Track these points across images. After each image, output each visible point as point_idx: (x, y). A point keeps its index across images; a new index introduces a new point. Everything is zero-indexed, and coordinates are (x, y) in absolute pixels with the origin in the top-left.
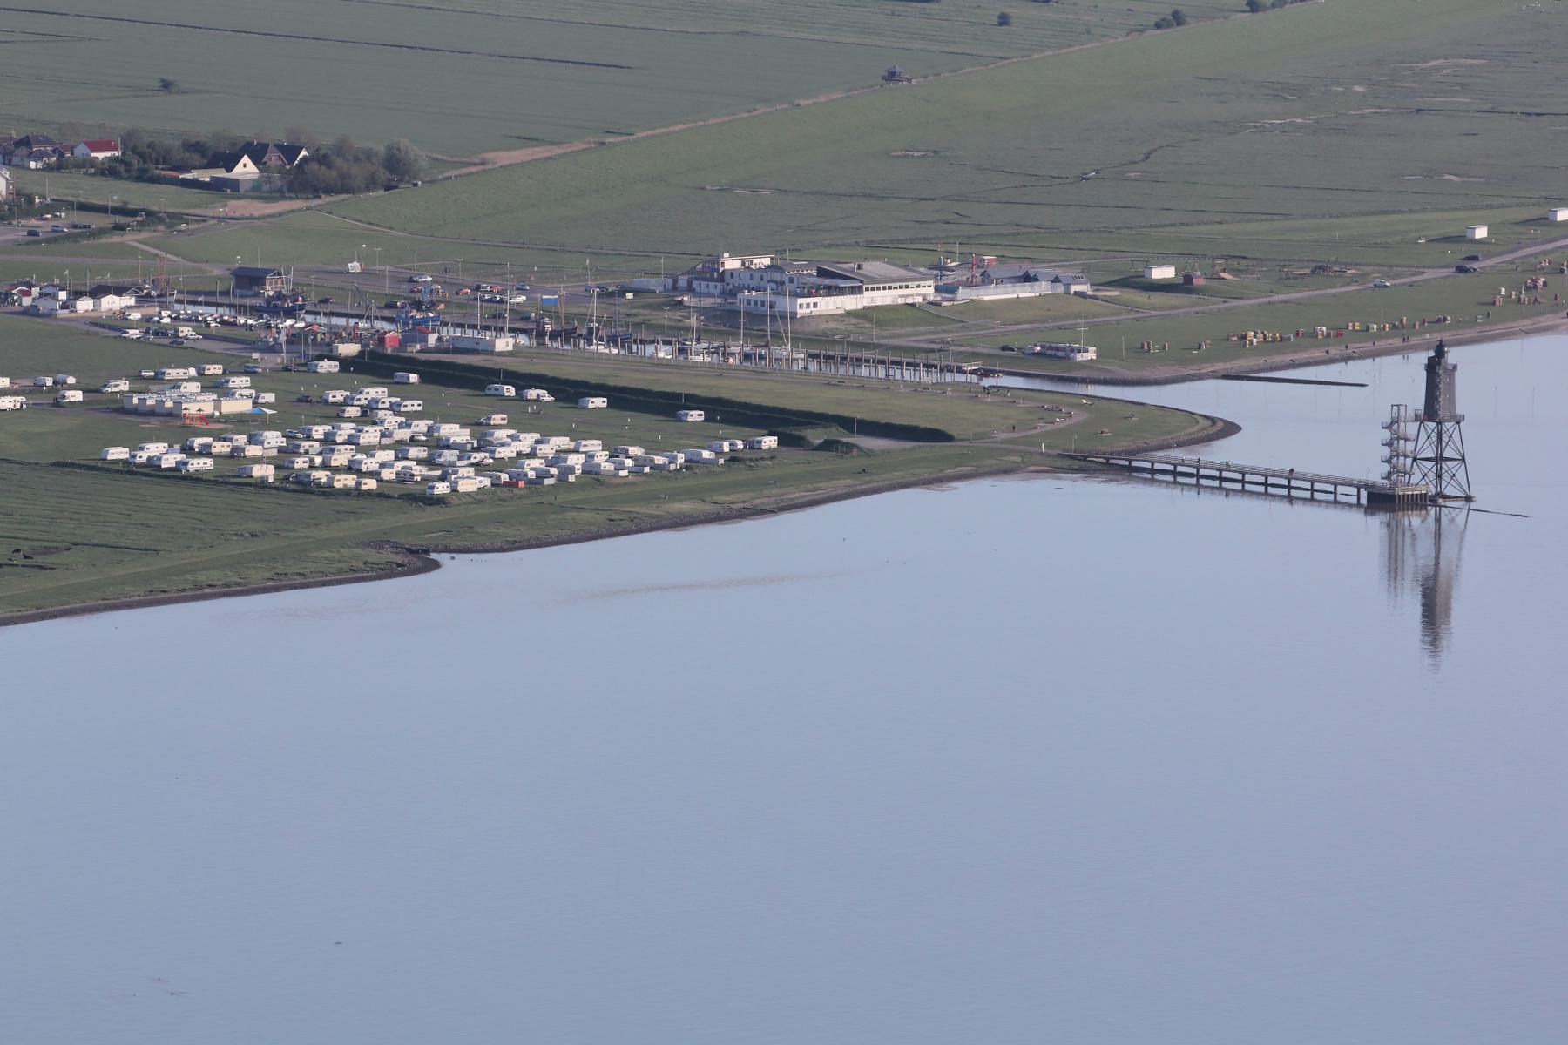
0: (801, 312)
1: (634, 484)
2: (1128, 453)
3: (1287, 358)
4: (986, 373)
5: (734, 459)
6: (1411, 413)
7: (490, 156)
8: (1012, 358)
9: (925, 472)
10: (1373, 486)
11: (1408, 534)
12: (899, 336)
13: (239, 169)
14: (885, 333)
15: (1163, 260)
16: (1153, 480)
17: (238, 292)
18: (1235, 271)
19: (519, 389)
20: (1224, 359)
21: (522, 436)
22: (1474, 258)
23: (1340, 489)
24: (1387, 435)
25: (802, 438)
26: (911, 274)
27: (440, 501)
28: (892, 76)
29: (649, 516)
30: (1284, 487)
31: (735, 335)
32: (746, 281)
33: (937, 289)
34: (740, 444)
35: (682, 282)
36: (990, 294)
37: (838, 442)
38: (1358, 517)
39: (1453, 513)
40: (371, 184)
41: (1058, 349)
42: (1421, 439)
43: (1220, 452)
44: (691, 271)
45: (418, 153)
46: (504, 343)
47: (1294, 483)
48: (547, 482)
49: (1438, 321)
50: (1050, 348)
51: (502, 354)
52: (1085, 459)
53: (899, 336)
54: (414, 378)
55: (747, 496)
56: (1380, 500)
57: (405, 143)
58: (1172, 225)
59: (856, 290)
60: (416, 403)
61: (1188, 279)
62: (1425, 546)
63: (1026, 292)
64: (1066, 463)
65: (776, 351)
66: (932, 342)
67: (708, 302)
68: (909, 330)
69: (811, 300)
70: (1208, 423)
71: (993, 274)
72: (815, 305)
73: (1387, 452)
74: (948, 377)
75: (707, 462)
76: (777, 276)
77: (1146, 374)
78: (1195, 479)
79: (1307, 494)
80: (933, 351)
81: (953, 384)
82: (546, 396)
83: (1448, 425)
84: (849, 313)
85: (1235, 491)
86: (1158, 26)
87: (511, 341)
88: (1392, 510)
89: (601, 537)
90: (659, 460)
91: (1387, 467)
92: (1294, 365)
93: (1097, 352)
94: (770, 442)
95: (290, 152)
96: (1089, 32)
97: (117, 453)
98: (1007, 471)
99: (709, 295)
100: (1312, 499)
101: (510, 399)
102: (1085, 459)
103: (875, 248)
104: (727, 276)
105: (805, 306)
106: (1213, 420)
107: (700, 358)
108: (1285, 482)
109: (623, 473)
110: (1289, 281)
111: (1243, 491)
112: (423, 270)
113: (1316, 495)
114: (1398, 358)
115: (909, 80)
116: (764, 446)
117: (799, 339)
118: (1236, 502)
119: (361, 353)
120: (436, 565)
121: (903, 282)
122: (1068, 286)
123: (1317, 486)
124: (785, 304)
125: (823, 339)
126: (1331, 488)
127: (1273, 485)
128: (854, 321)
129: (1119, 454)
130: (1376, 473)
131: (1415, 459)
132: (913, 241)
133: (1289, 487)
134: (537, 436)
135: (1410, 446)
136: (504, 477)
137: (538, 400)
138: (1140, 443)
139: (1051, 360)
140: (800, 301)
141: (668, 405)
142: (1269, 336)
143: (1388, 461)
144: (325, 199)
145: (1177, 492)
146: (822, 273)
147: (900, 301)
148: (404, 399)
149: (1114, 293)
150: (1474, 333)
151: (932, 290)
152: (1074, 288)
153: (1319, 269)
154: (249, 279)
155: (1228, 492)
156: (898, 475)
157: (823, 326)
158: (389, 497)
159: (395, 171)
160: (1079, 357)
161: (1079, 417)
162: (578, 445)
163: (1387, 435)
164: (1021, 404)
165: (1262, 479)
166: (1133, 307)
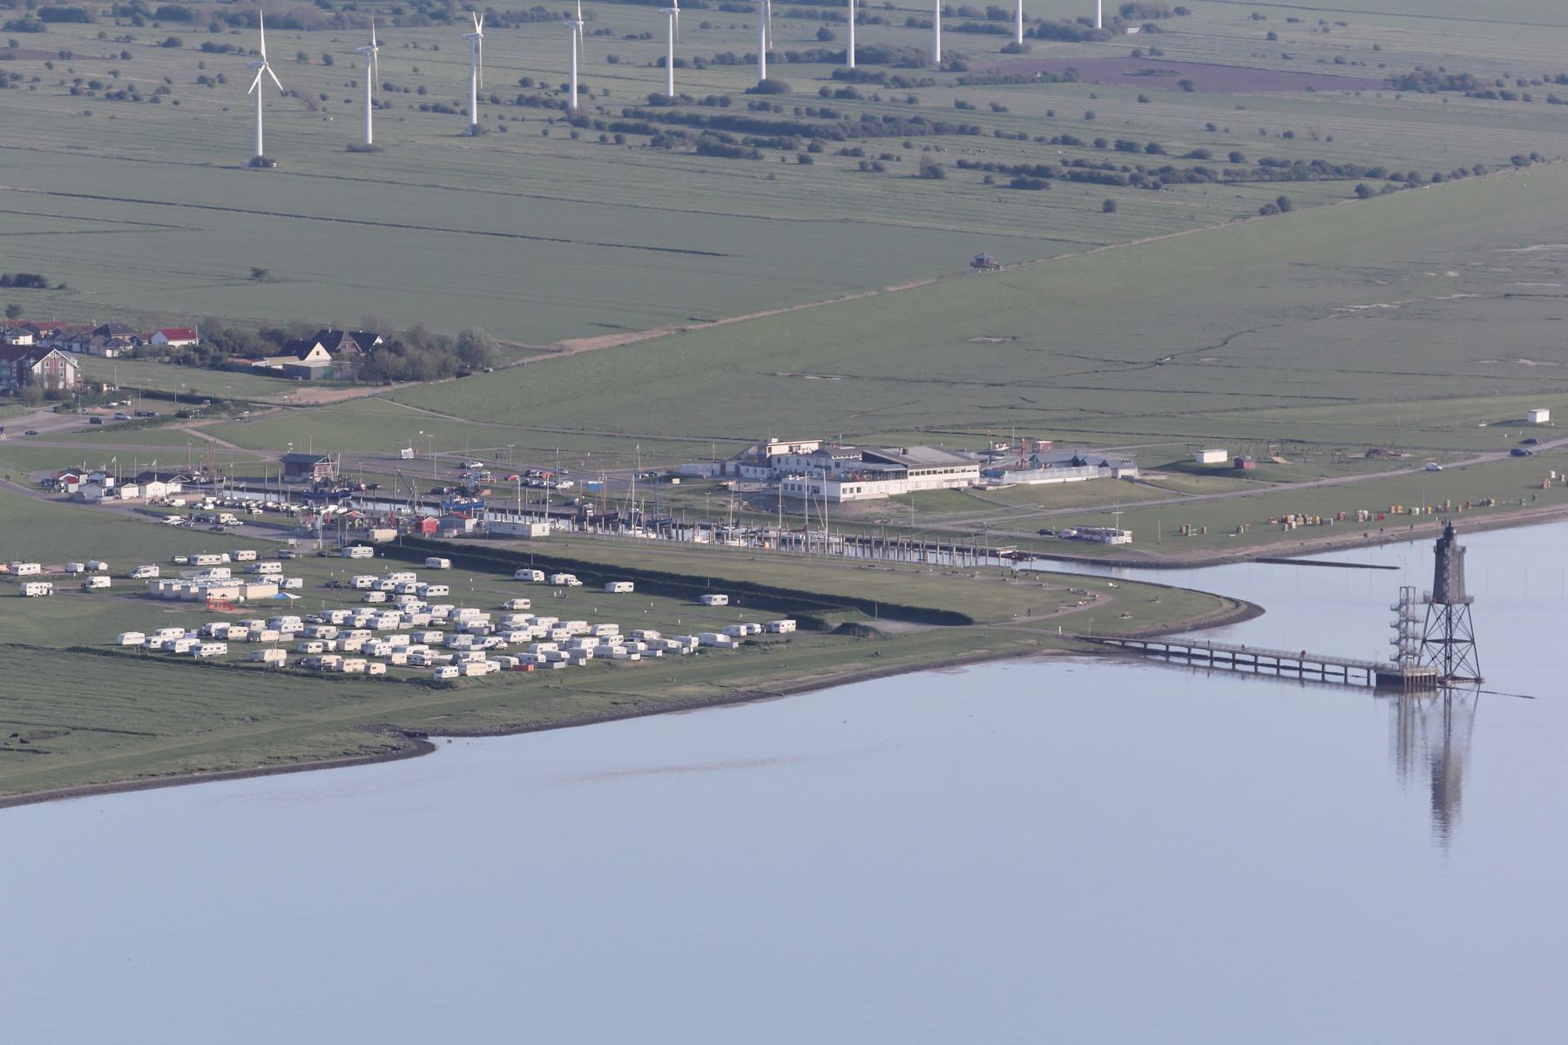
0: (844, 497)
1: (644, 667)
3: (1324, 541)
4: (1020, 557)
5: (748, 643)
6: (1420, 596)
8: (1049, 542)
9: (939, 655)
10: (1383, 668)
11: (1418, 716)
12: (940, 520)
13: (312, 356)
15: (1216, 444)
19: (548, 573)
20: (1260, 543)
21: (540, 620)
22: (1531, 442)
23: (1351, 671)
24: (1395, 617)
26: (957, 459)
27: (448, 685)
28: (980, 263)
29: (655, 700)
30: (1296, 669)
31: (774, 520)
32: (793, 465)
33: (984, 474)
34: (757, 628)
35: (730, 467)
36: (1037, 479)
38: (1368, 698)
39: (1463, 694)
40: (443, 370)
41: (1094, 533)
42: (1430, 621)
43: (1242, 635)
44: (737, 458)
45: (489, 338)
46: (540, 529)
47: (1305, 665)
48: (557, 665)
49: (1482, 504)
50: (1087, 532)
51: (538, 539)
52: (1101, 642)
53: (940, 520)
54: (445, 563)
56: (1389, 682)
58: (1236, 410)
59: (900, 475)
60: (442, 587)
61: (1239, 463)
62: (1435, 728)
63: (1074, 476)
64: (1082, 645)
66: (968, 525)
67: (754, 487)
68: (951, 514)
69: (855, 485)
70: (1232, 605)
72: (859, 490)
73: (1395, 634)
75: (721, 646)
76: (823, 462)
77: (1179, 557)
78: (1209, 661)
80: (969, 535)
82: (573, 581)
84: (893, 498)
86: (1263, 212)
93: (1133, 536)
94: (788, 626)
95: (364, 340)
97: (133, 638)
99: (756, 480)
101: (539, 583)
102: (1101, 642)
103: (932, 433)
104: (774, 462)
105: (848, 491)
106: (1237, 603)
107: (735, 543)
108: (1297, 665)
109: (635, 657)
116: (782, 630)
119: (397, 538)
121: (948, 466)
122: (1115, 470)
124: (826, 489)
125: (865, 523)
126: (1342, 670)
127: (1226, 660)
128: (898, 505)
129: (1135, 637)
130: (1385, 655)
131: (1424, 641)
132: (973, 426)
133: (1301, 670)
134: (555, 620)
135: (1419, 628)
136: (514, 661)
137: (566, 585)
139: (1087, 543)
140: (843, 485)
141: (692, 589)
142: (1310, 520)
143: (1397, 643)
144: (395, 386)
147: (946, 486)
148: (430, 584)
149: (1162, 477)
150: (1516, 516)
151: (977, 474)
152: (1122, 472)
153: (1372, 453)
154: (298, 465)
155: (1244, 674)
156: (911, 659)
157: (866, 510)
158: (397, 681)
159: (468, 358)
160: (1115, 541)
161: (1103, 599)
162: (595, 629)
163: (1395, 617)
164: (1047, 587)
165: (1274, 662)
166: (1180, 491)
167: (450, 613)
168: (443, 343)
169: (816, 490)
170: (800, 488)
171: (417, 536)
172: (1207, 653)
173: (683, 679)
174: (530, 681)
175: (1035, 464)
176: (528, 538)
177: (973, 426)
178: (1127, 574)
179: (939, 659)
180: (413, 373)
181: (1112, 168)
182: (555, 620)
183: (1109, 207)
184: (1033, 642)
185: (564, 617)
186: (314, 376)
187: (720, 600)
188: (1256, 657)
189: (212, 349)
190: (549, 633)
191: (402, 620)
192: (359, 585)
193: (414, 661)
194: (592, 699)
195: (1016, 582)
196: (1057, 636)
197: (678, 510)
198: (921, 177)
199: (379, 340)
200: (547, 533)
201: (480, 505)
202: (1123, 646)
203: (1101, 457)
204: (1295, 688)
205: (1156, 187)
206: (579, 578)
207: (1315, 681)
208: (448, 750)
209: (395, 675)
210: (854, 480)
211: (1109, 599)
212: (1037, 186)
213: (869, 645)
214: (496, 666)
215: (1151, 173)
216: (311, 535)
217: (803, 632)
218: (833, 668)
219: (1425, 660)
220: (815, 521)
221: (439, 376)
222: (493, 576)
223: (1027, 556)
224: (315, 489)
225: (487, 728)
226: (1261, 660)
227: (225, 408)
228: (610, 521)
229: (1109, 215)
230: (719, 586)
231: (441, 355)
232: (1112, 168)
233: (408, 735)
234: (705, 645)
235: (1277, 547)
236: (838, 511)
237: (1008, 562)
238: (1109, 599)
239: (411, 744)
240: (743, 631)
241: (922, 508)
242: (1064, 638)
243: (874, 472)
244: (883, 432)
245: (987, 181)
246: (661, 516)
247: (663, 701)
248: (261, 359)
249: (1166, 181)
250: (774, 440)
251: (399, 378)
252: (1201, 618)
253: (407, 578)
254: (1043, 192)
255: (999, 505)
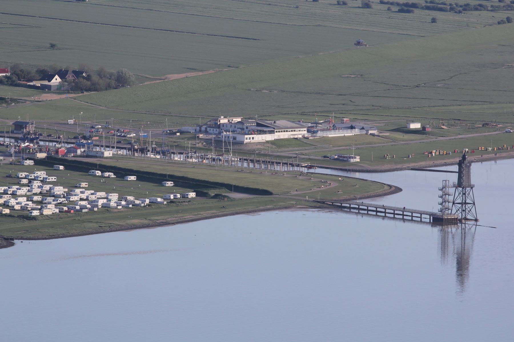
0: (246, 141)
1: (122, 212)
2: (340, 201)
3: (443, 162)
4: (310, 167)
6: (451, 184)
7: (169, 76)
8: (326, 161)
9: (250, 208)
11: (450, 236)
12: (285, 151)
13: (54, 80)
14: (280, 150)
16: (350, 212)
17: (15, 132)
18: (449, 125)
19: (102, 172)
20: (415, 162)
21: (86, 192)
23: (423, 216)
24: (441, 193)
25: (207, 193)
26: (297, 125)
27: (34, 218)
28: (358, 43)
29: (118, 225)
30: (402, 215)
31: (211, 150)
32: (229, 128)
34: (179, 196)
35: (203, 129)
36: (332, 134)
37: (220, 195)
38: (429, 227)
40: (108, 87)
41: (344, 157)
43: (390, 201)
44: (206, 124)
45: (128, 72)
46: (108, 153)
47: (405, 213)
48: (84, 211)
50: (341, 157)
51: (107, 158)
52: (324, 203)
53: (285, 151)
54: (62, 167)
55: (163, 217)
56: (437, 221)
57: (125, 70)
58: (438, 106)
59: (272, 132)
60: (54, 178)
62: (458, 240)
63: (349, 133)
65: (226, 156)
67: (210, 137)
68: (291, 149)
69: (251, 136)
70: (388, 188)
71: (337, 126)
72: (253, 138)
73: (440, 200)
74: (296, 169)
77: (379, 168)
78: (381, 213)
79: (410, 218)
81: (288, 172)
82: (112, 175)
83: (468, 189)
84: (267, 142)
85: (364, 214)
87: (111, 152)
88: (442, 225)
89: (92, 234)
90: (137, 202)
91: (440, 206)
92: (446, 165)
93: (360, 159)
94: (192, 195)
95: (77, 74)
96: (468, 26)
98: (286, 208)
100: (394, 218)
101: (99, 176)
102: (324, 203)
103: (285, 115)
104: (221, 126)
105: (248, 139)
108: (401, 213)
110: (472, 129)
111: (368, 214)
112: (99, 123)
113: (414, 218)
114: (493, 162)
115: (366, 45)
117: (235, 152)
118: (386, 222)
119: (47, 157)
120: (13, 244)
121: (293, 129)
123: (414, 215)
124: (239, 138)
125: (251, 152)
127: (410, 216)
128: (270, 145)
129: (337, 201)
130: (436, 209)
131: (454, 203)
132: (321, 112)
133: (403, 215)
134: (93, 192)
136: (65, 208)
137: (109, 177)
138: (352, 196)
140: (246, 136)
141: (155, 179)
142: (441, 152)
143: (441, 204)
144: (85, 93)
145: (359, 217)
146: (258, 125)
147: (292, 137)
148: (49, 176)
149: (387, 134)
151: (306, 132)
152: (370, 132)
153: (485, 125)
154: (19, 126)
156: (238, 209)
157: (255, 147)
158: (14, 217)
159: (121, 81)
160: (352, 160)
161: (334, 185)
162: (108, 196)
163: (441, 193)
165: (392, 212)
166: (394, 140)
167: (50, 188)
168: (111, 75)
169: (235, 138)
170: (228, 137)
171: (56, 156)
172: (384, 210)
173: (135, 217)
174: (70, 217)
175: (334, 128)
176: (103, 157)
177: (321, 112)
178: (358, 175)
179: (250, 209)
180: (93, 88)
181: (445, 4)
182: (93, 192)
183: (434, 21)
184: (294, 202)
185: (97, 191)
186: (52, 90)
187: (170, 184)
188: (333, 203)
189: (14, 78)
190: (87, 197)
191: (29, 191)
192: (20, 176)
193: (24, 209)
194: (91, 225)
195: (301, 178)
196: (306, 200)
197: (172, 146)
198: (362, 8)
199: (84, 74)
200: (111, 155)
201: (92, 143)
202: (332, 205)
203: (362, 124)
204: (400, 224)
205: (460, 12)
206: (114, 175)
207: (409, 220)
208: (21, 246)
209: (12, 214)
210: (252, 134)
211: (336, 184)
212: (409, 12)
213: (225, 203)
214: (57, 211)
215: (461, 6)
216: (11, 156)
217: (199, 198)
218: (201, 213)
219: (454, 211)
220: (227, 151)
221: (106, 89)
222: (81, 173)
223: (313, 166)
224: (24, 136)
225: (40, 237)
226: (387, 211)
227: (6, 102)
228: (143, 151)
229: (434, 24)
230: (171, 178)
231: (108, 81)
232: (445, 4)
233: (5, 239)
234: (153, 202)
235: (423, 164)
236: (242, 147)
237: (305, 170)
238: (336, 184)
239: (5, 243)
240: (172, 197)
241: (279, 146)
242: (308, 201)
243: (260, 131)
244: (282, 114)
245: (389, 9)
246: (166, 149)
247: (122, 225)
248: (32, 82)
249: (465, 10)
250: (222, 117)
251: (89, 90)
252: (372, 193)
253: (42, 174)
254: (411, 14)
255: (313, 145)
